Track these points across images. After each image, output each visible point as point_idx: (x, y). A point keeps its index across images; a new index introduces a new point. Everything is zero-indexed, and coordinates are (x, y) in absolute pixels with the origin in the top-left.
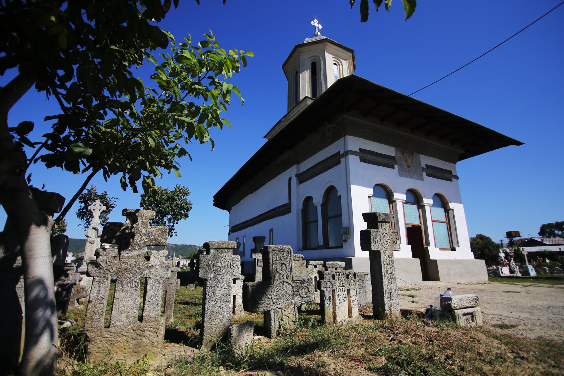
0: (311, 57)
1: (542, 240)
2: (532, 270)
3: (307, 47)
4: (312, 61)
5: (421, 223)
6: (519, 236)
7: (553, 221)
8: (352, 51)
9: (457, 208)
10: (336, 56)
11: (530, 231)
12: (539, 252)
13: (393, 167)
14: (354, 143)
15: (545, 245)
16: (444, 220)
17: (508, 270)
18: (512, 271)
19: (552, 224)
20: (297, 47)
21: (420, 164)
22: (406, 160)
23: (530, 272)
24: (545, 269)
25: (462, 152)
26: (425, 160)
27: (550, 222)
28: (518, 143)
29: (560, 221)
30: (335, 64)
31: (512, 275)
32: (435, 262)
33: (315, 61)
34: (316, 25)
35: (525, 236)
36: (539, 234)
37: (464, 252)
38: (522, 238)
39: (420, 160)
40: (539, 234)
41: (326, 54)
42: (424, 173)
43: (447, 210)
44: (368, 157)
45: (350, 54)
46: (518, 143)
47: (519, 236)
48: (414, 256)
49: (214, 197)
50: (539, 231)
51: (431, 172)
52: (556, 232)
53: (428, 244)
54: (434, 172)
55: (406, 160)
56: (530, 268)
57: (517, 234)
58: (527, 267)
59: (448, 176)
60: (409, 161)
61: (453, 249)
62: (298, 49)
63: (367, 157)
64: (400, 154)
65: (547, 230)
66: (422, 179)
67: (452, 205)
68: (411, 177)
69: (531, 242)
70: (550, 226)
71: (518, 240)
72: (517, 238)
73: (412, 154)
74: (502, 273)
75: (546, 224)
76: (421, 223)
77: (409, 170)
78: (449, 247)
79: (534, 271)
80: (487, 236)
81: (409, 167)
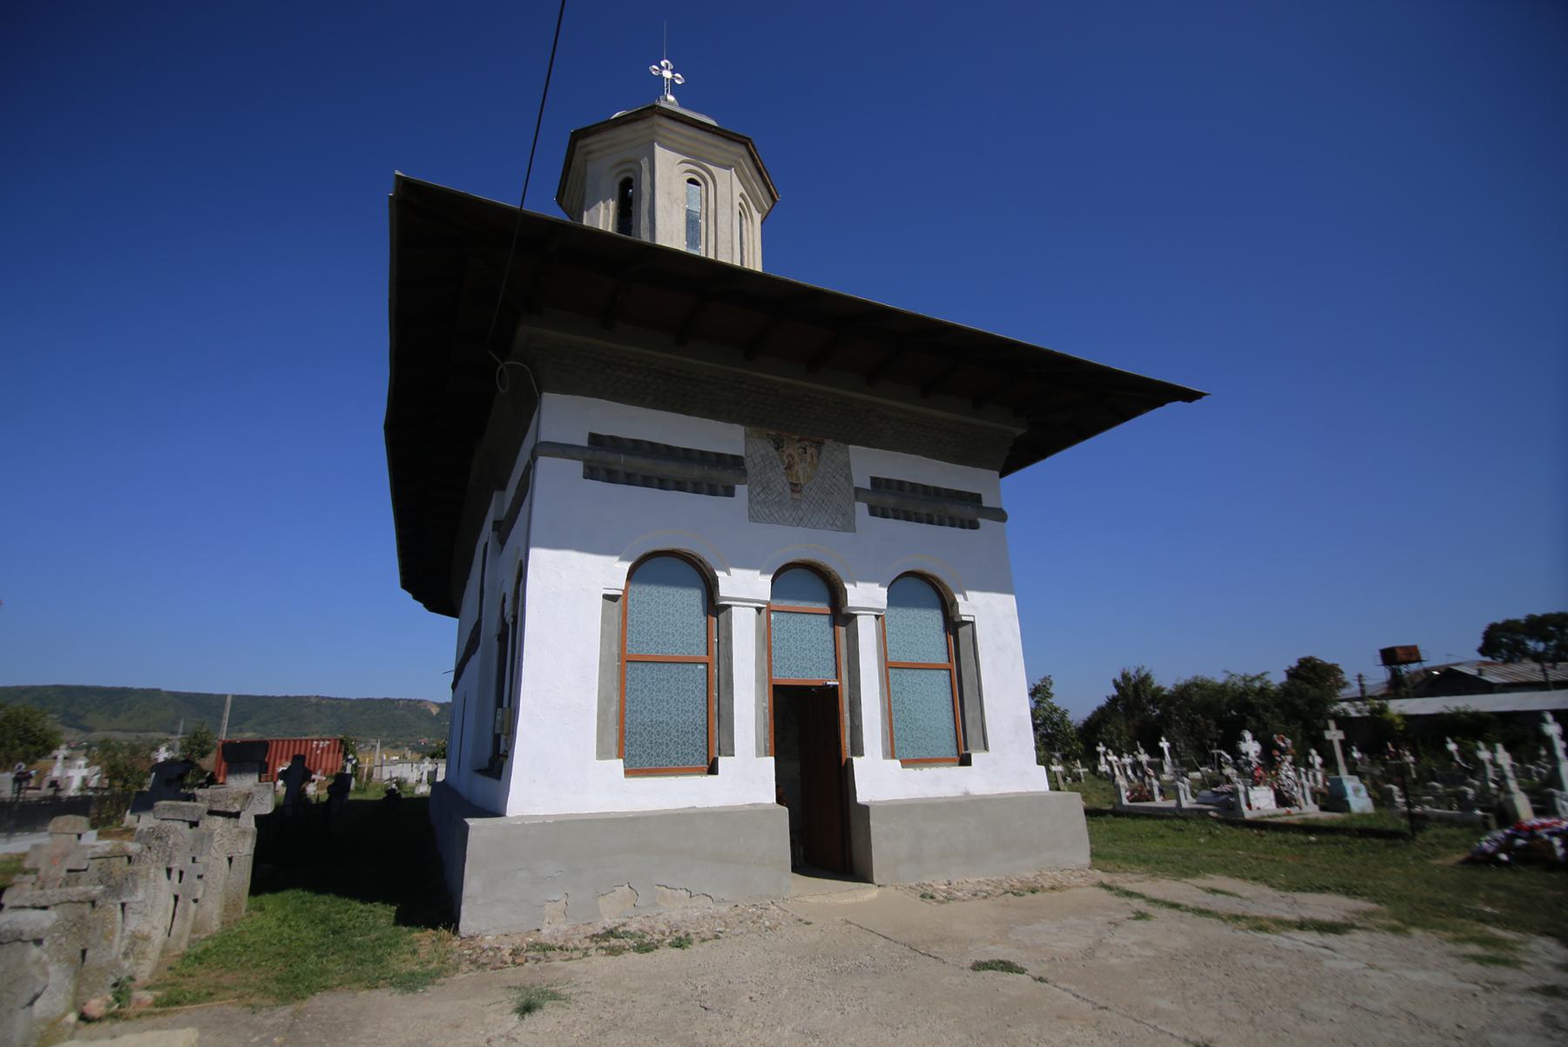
0: (620, 164)
1: (1480, 671)
2: (1356, 791)
3: (604, 136)
4: (623, 176)
5: (837, 676)
6: (1419, 660)
7: (1519, 614)
8: (744, 141)
9: (992, 615)
10: (694, 156)
11: (1452, 646)
12: (1441, 715)
13: (729, 492)
14: (565, 417)
15: (1490, 688)
16: (940, 657)
17: (1272, 794)
18: (1282, 799)
19: (1516, 622)
20: (578, 136)
21: (848, 478)
22: (789, 467)
23: (1351, 798)
24: (1391, 791)
25: (1020, 432)
26: (868, 463)
27: (1512, 617)
28: (1190, 396)
29: (1539, 612)
30: (691, 181)
31: (1283, 810)
32: (865, 809)
33: (629, 175)
34: (667, 74)
35: (1434, 658)
36: (1482, 651)
37: (1010, 765)
38: (1426, 665)
39: (848, 465)
40: (1482, 651)
41: (658, 150)
42: (861, 508)
43: (953, 625)
44: (622, 461)
45: (741, 150)
46: (1190, 396)
47: (1419, 660)
48: (779, 800)
49: (407, 584)
50: (1479, 642)
51: (890, 501)
52: (1531, 644)
53: (858, 750)
54: (896, 500)
55: (789, 467)
56: (1351, 784)
57: (1412, 654)
58: (1340, 781)
59: (962, 511)
60: (801, 469)
61: (965, 761)
62: (580, 143)
63: (609, 461)
64: (764, 448)
65: (1501, 641)
66: (849, 526)
67: (970, 604)
68: (799, 522)
69: (1450, 681)
70: (1509, 627)
71: (1417, 673)
72: (1414, 667)
73: (819, 445)
74: (1249, 805)
75: (1499, 621)
76: (837, 676)
77: (793, 500)
78: (951, 751)
79: (1364, 793)
80: (1329, 660)
81: (795, 487)
